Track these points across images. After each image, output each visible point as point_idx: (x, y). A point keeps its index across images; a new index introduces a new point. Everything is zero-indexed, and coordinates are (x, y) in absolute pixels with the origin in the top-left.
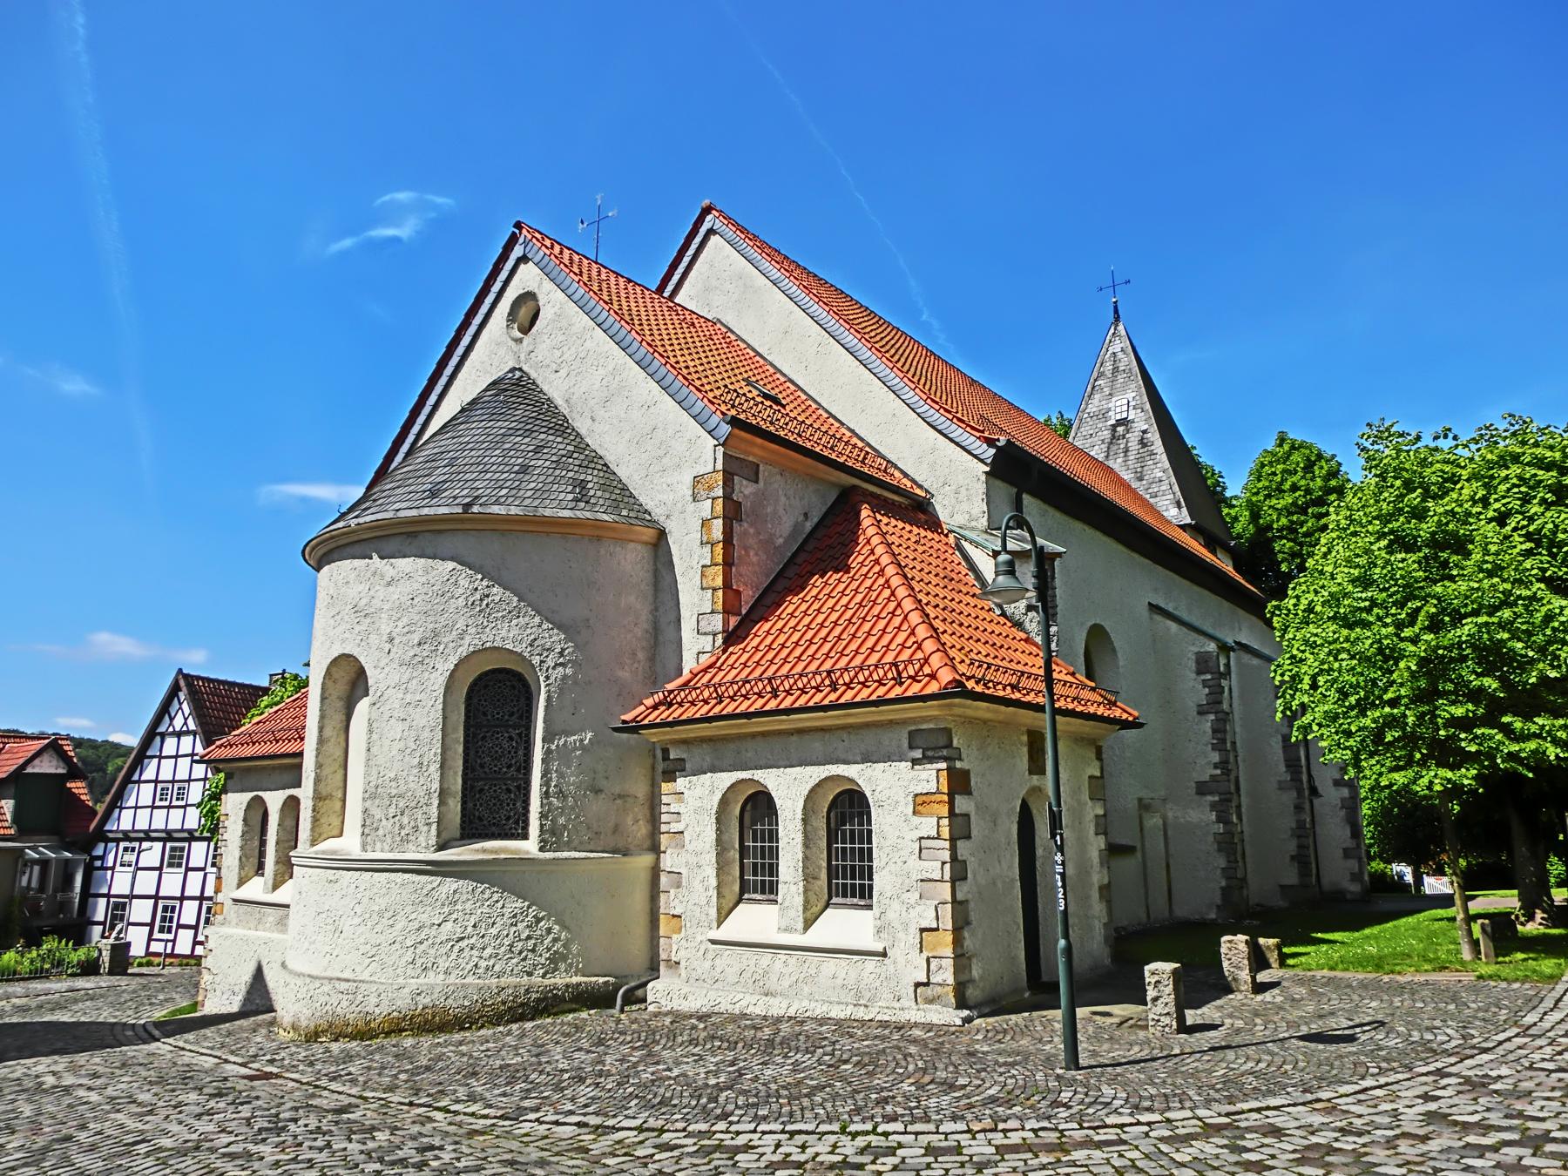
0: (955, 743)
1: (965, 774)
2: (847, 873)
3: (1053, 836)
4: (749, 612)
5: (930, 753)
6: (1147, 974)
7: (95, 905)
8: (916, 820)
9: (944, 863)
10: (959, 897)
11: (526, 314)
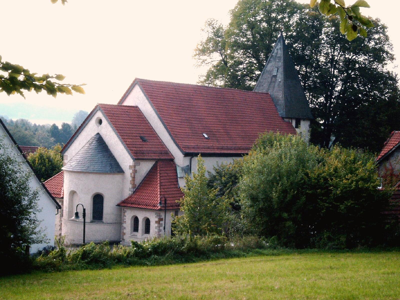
11: (100, 122)
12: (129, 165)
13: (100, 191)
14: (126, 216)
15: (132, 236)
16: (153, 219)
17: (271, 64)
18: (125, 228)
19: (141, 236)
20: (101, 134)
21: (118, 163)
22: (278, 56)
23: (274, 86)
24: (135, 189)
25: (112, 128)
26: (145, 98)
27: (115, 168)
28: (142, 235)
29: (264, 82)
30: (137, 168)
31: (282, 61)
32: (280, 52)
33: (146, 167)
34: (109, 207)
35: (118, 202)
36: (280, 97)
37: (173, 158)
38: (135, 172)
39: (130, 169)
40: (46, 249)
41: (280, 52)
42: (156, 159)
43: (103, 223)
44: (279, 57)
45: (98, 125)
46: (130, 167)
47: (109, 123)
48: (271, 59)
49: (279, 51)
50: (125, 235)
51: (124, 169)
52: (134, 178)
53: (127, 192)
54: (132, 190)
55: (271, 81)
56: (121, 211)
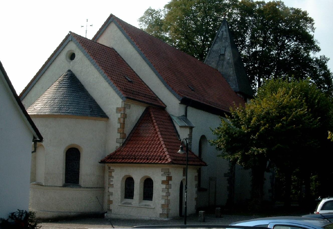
0: (170, 171)
1: (171, 177)
2: (148, 194)
3: (185, 190)
4: (127, 138)
5: (165, 173)
6: (199, 212)
7: (331, 210)
8: (162, 185)
9: (166, 193)
10: (169, 199)
11: (72, 57)
12: (115, 107)
13: (76, 142)
14: (113, 177)
15: (124, 204)
16: (158, 178)
17: (218, 44)
18: (112, 194)
19: (138, 203)
20: (74, 72)
21: (99, 106)
22: (224, 37)
23: (223, 64)
24: (124, 140)
25: (90, 61)
26: (123, 36)
27: (96, 111)
28: (140, 202)
29: (211, 61)
30: (128, 111)
31: (229, 41)
32: (226, 34)
33: (136, 111)
34: (88, 168)
35: (100, 159)
36: (231, 73)
37: (164, 106)
38: (125, 116)
39: (117, 112)
40: (15, 216)
41: (226, 34)
42: (147, 103)
43: (80, 187)
44: (225, 38)
45: (69, 60)
46: (118, 110)
47: (85, 55)
48: (217, 40)
49: (225, 33)
50: (112, 204)
51: (108, 114)
52: (123, 125)
53: (113, 143)
54: (121, 141)
55: (219, 60)
56: (104, 170)
